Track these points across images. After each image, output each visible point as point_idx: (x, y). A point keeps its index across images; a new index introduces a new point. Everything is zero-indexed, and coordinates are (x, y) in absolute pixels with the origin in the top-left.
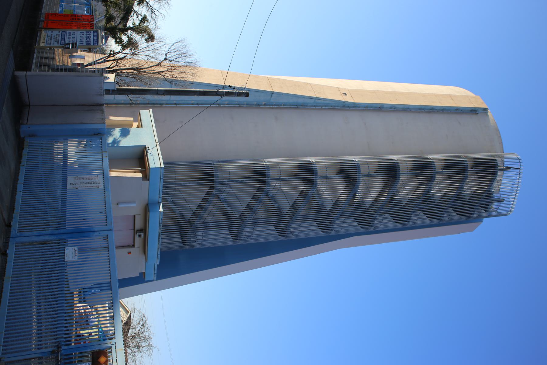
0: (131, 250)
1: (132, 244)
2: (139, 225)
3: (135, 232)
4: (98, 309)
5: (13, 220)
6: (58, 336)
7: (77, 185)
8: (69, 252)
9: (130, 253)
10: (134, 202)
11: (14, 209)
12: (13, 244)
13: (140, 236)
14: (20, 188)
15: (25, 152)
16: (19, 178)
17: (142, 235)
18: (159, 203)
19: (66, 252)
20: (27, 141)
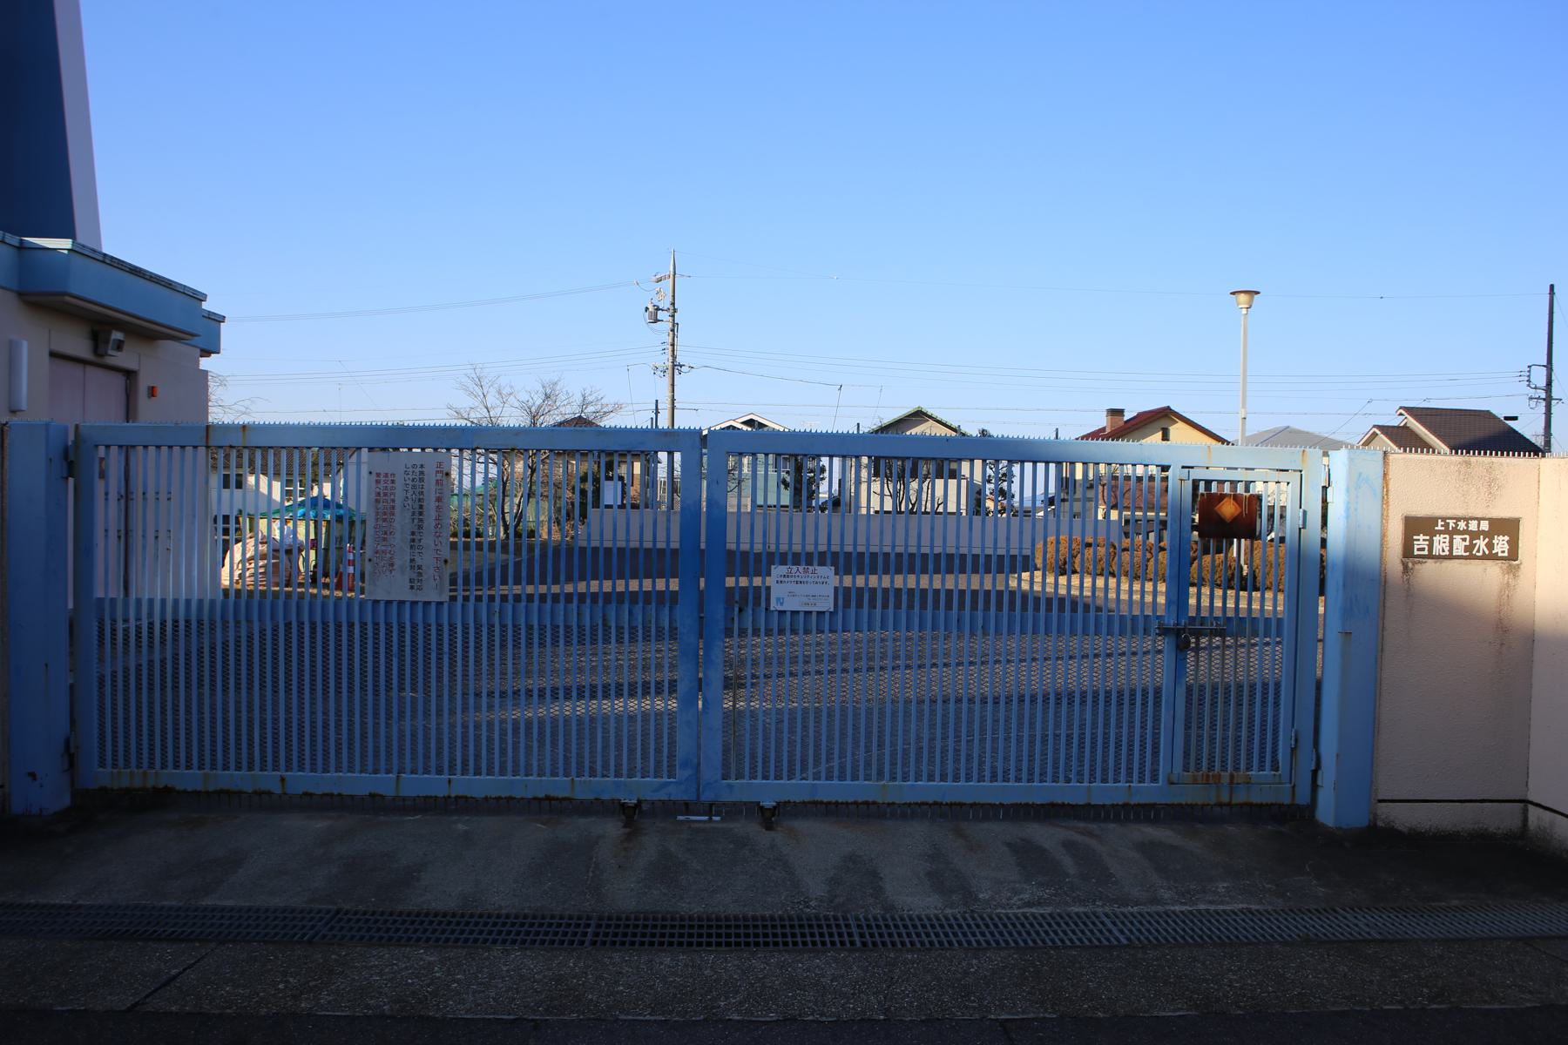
0: (143, 384)
1: (119, 381)
2: (78, 344)
3: (97, 361)
4: (760, 501)
5: (605, 797)
6: (218, 619)
7: (427, 560)
8: (792, 594)
9: (152, 392)
10: (12, 348)
11: (1053, 805)
12: (730, 786)
13: (119, 346)
14: (382, 783)
15: (187, 779)
16: (362, 791)
17: (117, 335)
18: (22, 247)
19: (789, 606)
20: (101, 776)
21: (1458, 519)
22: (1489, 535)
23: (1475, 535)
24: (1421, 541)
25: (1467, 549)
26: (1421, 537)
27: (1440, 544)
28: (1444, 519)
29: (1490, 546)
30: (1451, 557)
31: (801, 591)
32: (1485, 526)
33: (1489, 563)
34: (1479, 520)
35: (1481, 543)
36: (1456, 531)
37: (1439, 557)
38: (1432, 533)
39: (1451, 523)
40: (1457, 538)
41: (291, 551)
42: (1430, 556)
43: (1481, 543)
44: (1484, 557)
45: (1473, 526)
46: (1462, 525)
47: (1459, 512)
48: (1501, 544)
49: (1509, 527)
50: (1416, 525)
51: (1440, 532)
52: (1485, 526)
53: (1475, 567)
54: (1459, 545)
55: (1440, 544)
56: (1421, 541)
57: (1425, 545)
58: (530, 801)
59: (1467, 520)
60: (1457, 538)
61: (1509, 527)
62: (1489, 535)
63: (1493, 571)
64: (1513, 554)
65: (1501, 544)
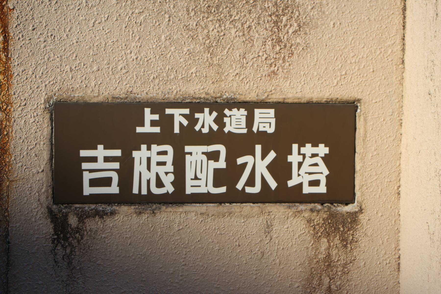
21: (196, 106)
22: (278, 143)
23: (240, 145)
24: (99, 162)
25: (219, 177)
26: (100, 152)
27: (152, 167)
28: (158, 107)
29: (281, 169)
30: (179, 197)
31: (8, 240)
32: (266, 122)
33: (278, 211)
34: (250, 107)
35: (258, 164)
36: (191, 136)
37: (150, 201)
38: (129, 142)
39: (179, 116)
40: (195, 154)
41: (357, 226)
42: (126, 197)
43: (258, 164)
44: (266, 197)
45: (236, 121)
46: (206, 120)
47: (196, 89)
48: (309, 166)
49: (331, 124)
50: (79, 123)
51: (150, 140)
52: (266, 122)
53: (244, 225)
54: (201, 169)
55: (152, 167)
56: (99, 162)
57: (111, 170)
58: (349, 203)
59: (219, 106)
60: (195, 154)
61: (331, 124)
62: (278, 143)
63: (289, 234)
64: (342, 184)
65: (309, 166)
